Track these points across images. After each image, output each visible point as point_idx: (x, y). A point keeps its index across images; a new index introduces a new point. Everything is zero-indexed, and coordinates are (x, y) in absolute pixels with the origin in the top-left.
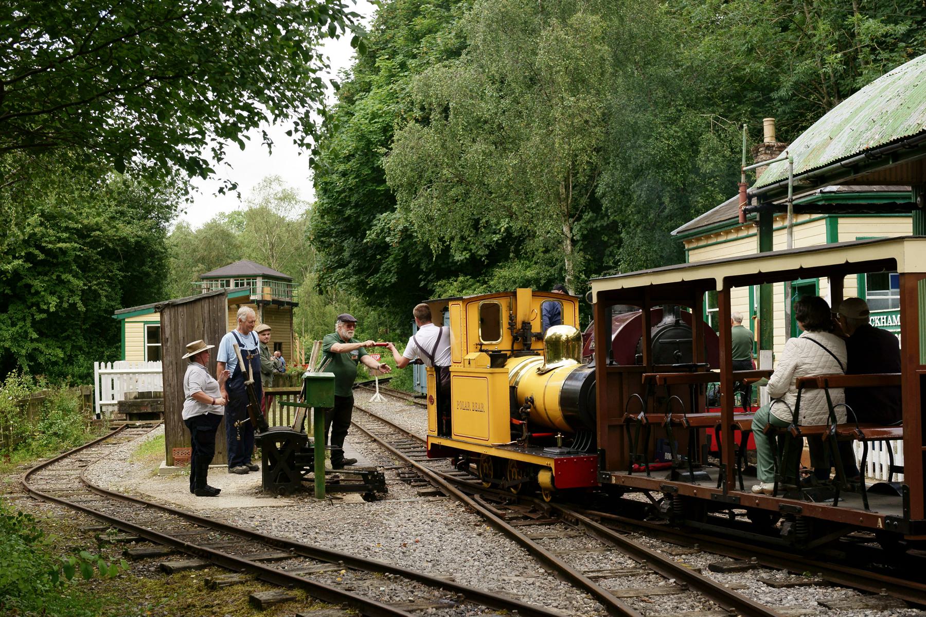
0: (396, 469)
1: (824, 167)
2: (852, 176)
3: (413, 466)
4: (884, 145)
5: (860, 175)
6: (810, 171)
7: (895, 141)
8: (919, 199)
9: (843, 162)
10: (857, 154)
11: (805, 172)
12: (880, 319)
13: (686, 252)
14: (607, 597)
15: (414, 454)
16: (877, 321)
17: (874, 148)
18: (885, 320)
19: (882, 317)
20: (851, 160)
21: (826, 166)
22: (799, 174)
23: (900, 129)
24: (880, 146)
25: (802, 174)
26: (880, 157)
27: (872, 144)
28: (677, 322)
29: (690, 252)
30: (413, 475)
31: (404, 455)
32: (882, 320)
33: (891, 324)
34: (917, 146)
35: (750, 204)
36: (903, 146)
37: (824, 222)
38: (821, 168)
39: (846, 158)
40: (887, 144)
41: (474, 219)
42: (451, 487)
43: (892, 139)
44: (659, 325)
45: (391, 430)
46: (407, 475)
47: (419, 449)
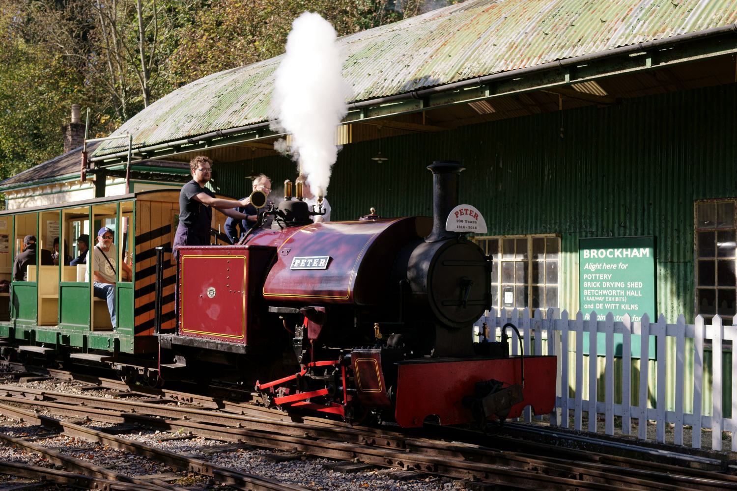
35: (89, 167)
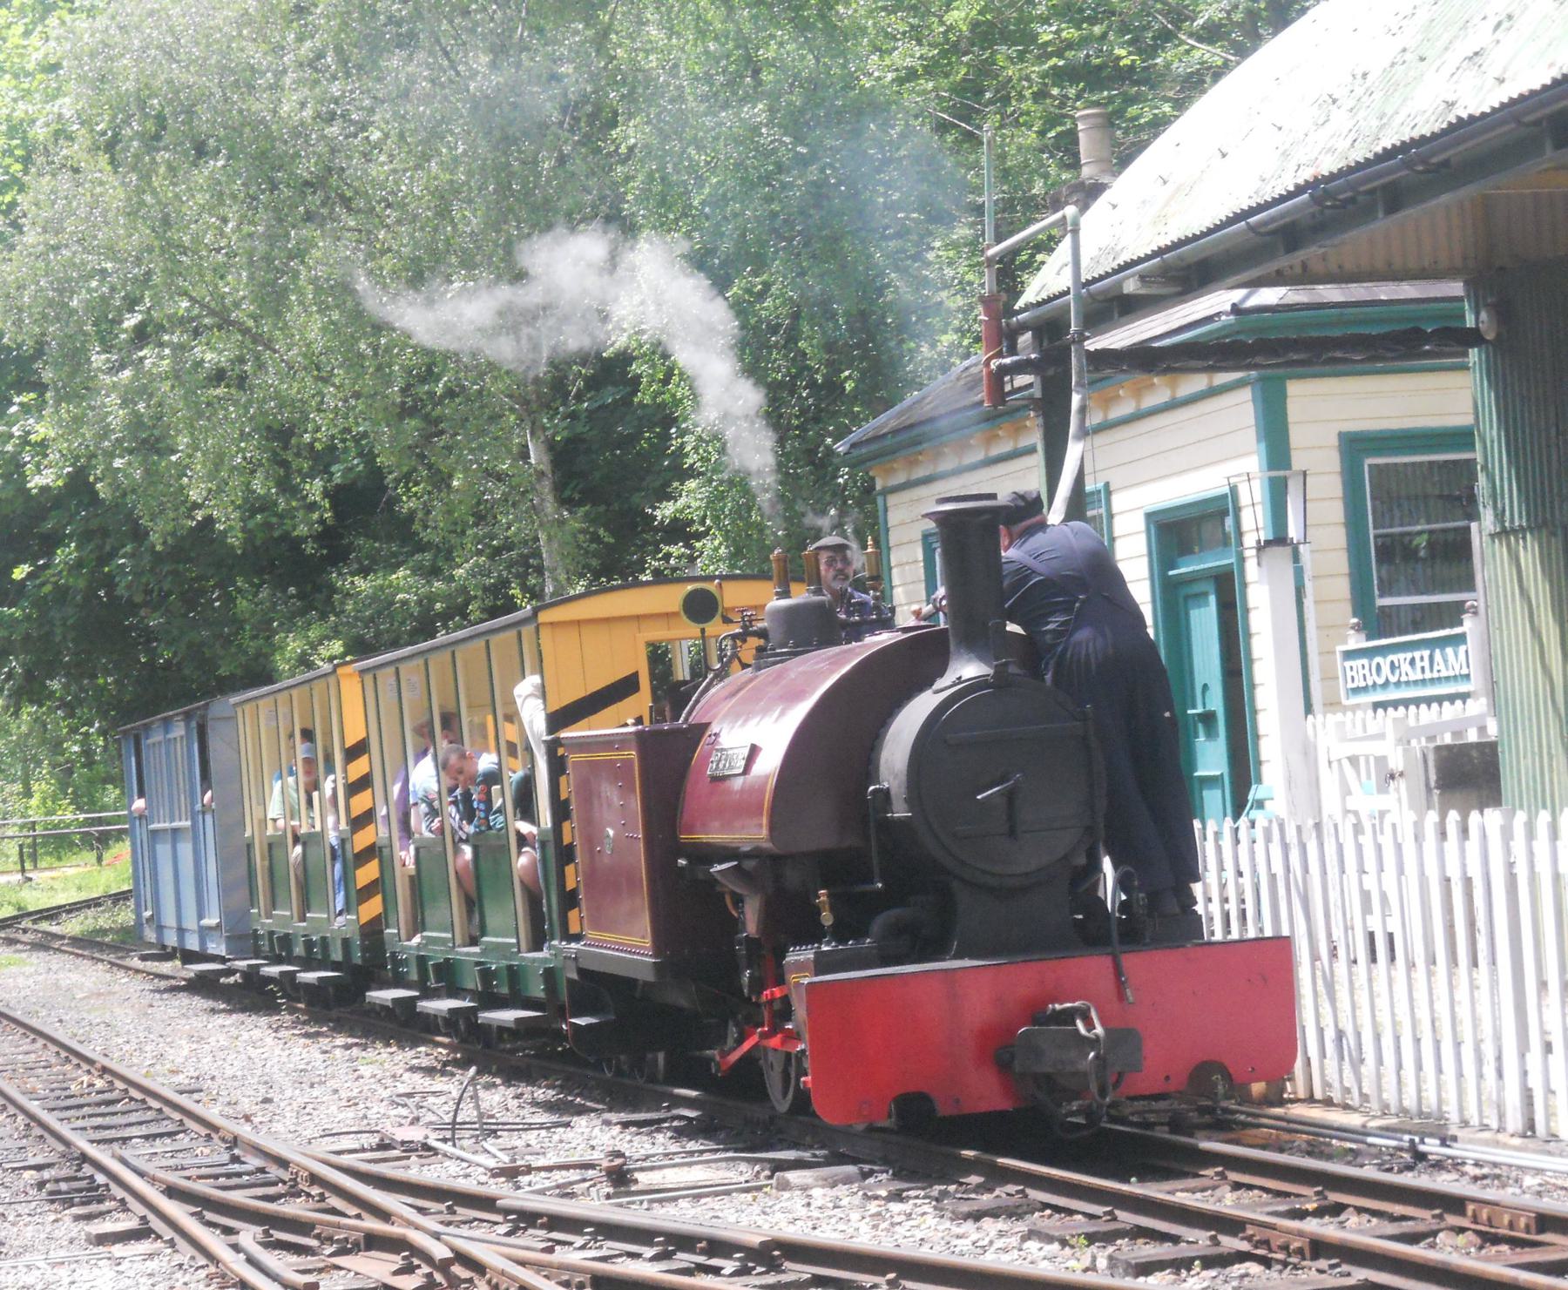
0: (39, 1168)
1: (1204, 235)
2: (1282, 262)
3: (85, 1158)
4: (1359, 166)
5: (1301, 255)
6: (1168, 249)
7: (1388, 154)
8: (1484, 315)
9: (1251, 220)
10: (1290, 195)
11: (1155, 254)
12: (1412, 662)
13: (880, 500)
14: (1427, 1259)
15: (99, 1121)
16: (1405, 667)
17: (1332, 177)
18: (1426, 664)
19: (1417, 654)
20: (1272, 211)
21: (1210, 231)
22: (1140, 261)
23: (1399, 119)
24: (1351, 170)
25: (1148, 258)
26: (1352, 200)
27: (1329, 165)
28: (1000, 671)
29: (892, 500)
30: (83, 1184)
31: (64, 1130)
32: (1419, 664)
33: (1444, 674)
34: (1445, 164)
35: (1013, 350)
36: (1407, 164)
37: (1246, 394)
38: (1196, 238)
39: (1260, 208)
40: (1368, 163)
41: (990, 262)
42: (177, 1210)
43: (1379, 149)
44: (939, 684)
45: (50, 1054)
46: (64, 1186)
47: (133, 1118)
